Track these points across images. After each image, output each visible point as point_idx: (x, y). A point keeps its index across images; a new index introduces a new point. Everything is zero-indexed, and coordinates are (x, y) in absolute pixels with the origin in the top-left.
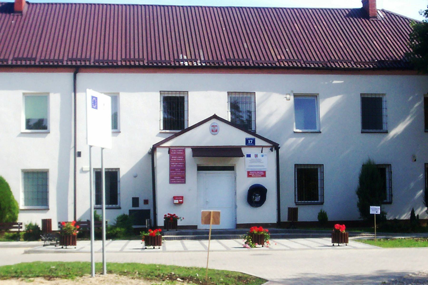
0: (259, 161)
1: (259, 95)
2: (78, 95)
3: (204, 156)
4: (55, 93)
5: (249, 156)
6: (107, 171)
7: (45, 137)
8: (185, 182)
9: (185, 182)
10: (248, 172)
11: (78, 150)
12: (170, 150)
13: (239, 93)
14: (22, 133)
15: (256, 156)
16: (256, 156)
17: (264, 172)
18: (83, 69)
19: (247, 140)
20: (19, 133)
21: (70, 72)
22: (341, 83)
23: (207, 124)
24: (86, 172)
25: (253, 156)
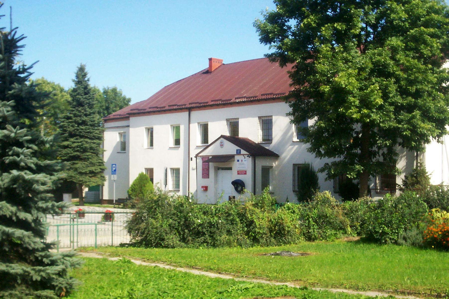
0: (243, 164)
1: (274, 118)
2: (191, 125)
3: (217, 162)
4: (182, 125)
5: (238, 161)
6: (263, 167)
7: (178, 150)
8: (209, 178)
9: (209, 178)
10: (238, 171)
11: (190, 157)
12: (203, 157)
13: (264, 116)
14: (170, 148)
15: (242, 161)
16: (242, 161)
17: (246, 171)
18: (193, 109)
19: (237, 150)
20: (168, 148)
21: (186, 111)
22: (176, 130)
23: (219, 142)
24: (195, 169)
25: (240, 161)
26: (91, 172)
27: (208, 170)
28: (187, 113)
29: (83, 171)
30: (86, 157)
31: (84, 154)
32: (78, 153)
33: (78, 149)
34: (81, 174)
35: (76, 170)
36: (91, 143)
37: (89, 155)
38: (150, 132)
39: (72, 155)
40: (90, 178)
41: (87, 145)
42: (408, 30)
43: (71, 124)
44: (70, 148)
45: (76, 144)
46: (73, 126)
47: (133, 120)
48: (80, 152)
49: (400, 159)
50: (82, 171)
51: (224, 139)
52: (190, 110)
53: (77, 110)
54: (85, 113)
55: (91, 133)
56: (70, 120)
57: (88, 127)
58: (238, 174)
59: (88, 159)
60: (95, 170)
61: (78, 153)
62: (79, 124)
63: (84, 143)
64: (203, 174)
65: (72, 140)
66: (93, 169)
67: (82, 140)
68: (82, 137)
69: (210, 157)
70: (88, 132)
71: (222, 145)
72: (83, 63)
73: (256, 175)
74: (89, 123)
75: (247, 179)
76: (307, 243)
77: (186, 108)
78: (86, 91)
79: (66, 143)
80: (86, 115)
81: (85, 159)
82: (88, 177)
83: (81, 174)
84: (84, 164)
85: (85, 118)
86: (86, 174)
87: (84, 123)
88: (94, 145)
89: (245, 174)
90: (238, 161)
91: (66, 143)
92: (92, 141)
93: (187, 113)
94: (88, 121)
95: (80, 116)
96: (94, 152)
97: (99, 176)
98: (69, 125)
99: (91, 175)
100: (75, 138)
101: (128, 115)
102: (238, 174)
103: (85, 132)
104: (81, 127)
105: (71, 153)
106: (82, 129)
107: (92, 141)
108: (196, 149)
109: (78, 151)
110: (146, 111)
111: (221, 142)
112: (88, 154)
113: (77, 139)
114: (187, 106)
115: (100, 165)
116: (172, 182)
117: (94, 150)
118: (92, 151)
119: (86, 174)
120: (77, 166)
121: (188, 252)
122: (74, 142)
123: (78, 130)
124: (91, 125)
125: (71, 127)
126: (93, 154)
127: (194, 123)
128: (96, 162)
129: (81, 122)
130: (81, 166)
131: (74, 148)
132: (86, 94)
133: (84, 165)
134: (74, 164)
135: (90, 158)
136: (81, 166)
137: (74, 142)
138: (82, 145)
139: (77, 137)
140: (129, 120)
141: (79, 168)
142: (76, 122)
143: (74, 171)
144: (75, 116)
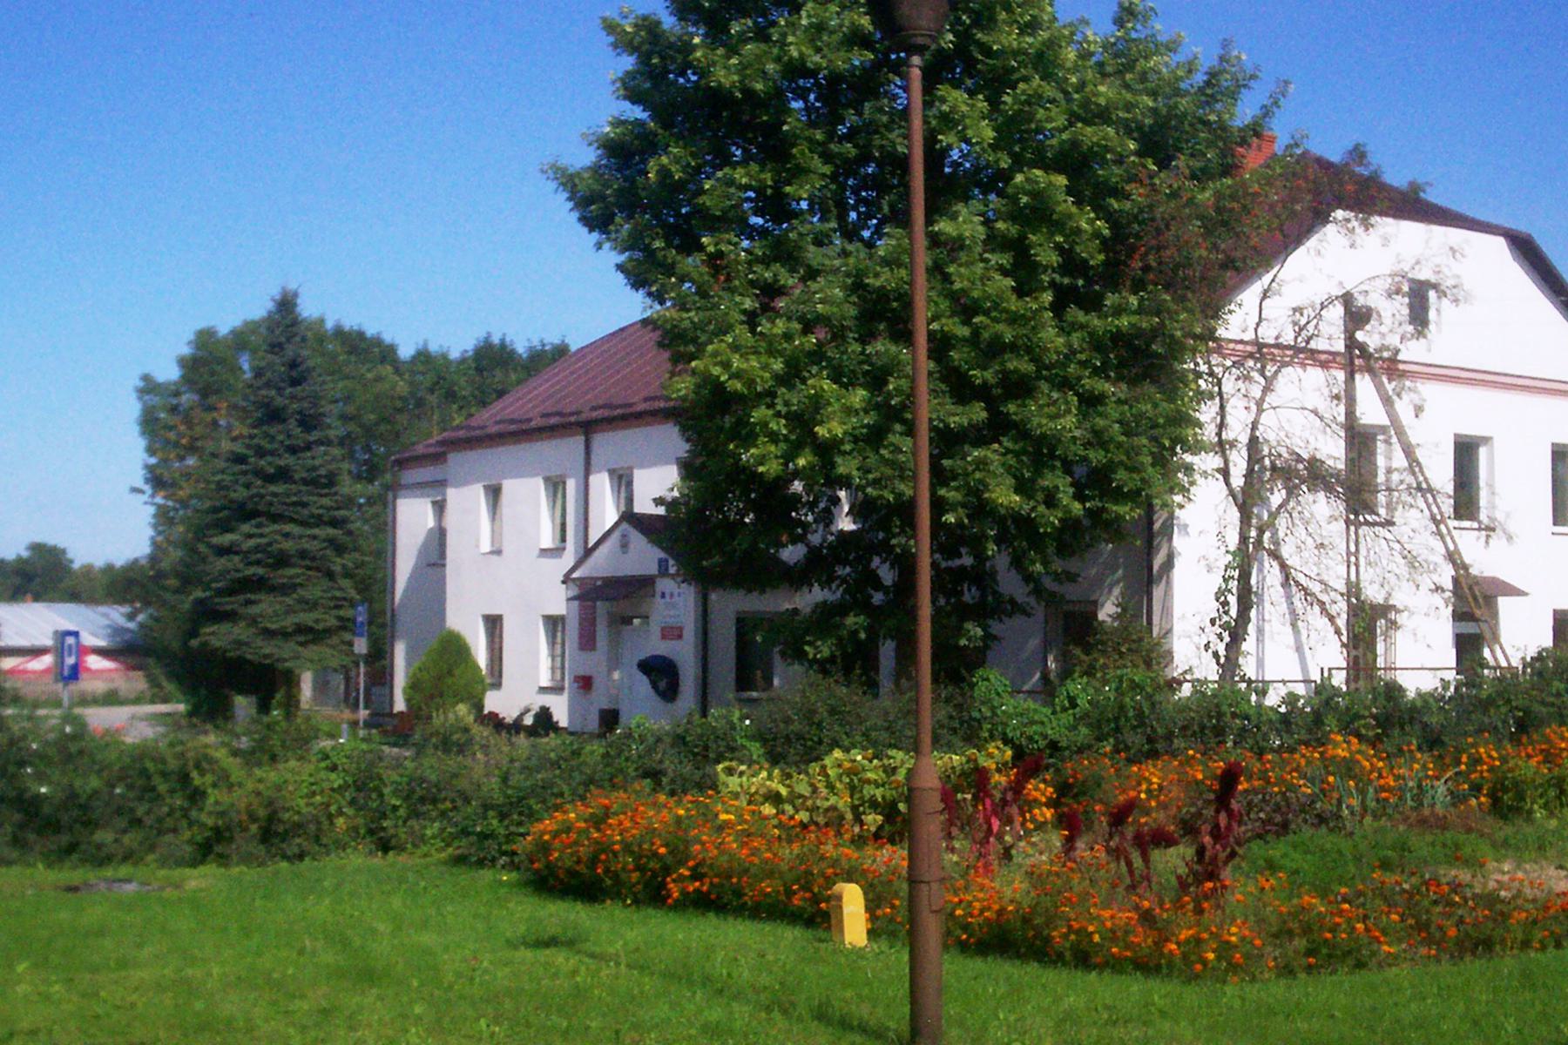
20: (537, 552)
25: (667, 596)
26: (301, 629)
27: (593, 623)
28: (581, 439)
29: (274, 627)
30: (285, 581)
31: (280, 572)
32: (260, 571)
33: (259, 556)
34: (269, 634)
35: (253, 621)
36: (301, 537)
37: (298, 576)
38: (623, 495)
39: (241, 575)
40: (300, 649)
41: (288, 545)
42: (1006, 176)
43: (242, 479)
44: (236, 553)
45: (252, 543)
46: (248, 486)
47: (454, 458)
48: (267, 566)
49: (1106, 590)
50: (269, 625)
51: (635, 527)
52: (588, 428)
53: (266, 435)
54: (287, 443)
55: (304, 505)
56: (244, 467)
57: (293, 486)
58: (664, 637)
59: (294, 587)
60: (317, 621)
61: (260, 571)
62: (269, 479)
63: (278, 537)
64: (580, 644)
65: (246, 528)
66: (307, 618)
67: (276, 527)
68: (276, 518)
69: (599, 583)
70: (295, 504)
71: (624, 546)
72: (292, 286)
73: (710, 646)
74: (297, 477)
75: (684, 653)
76: (377, 861)
77: (579, 424)
78: (294, 374)
79: (227, 539)
80: (293, 450)
81: (286, 589)
82: (292, 645)
83: (269, 634)
84: (280, 603)
85: (288, 460)
86: (284, 634)
87: (283, 475)
88: (315, 542)
89: (680, 637)
90: (663, 596)
91: (227, 539)
92: (309, 532)
93: (578, 441)
94: (297, 467)
95: (273, 453)
96: (314, 564)
97: (335, 640)
98: (237, 482)
99: (302, 639)
100: (253, 522)
101: (439, 449)
102: (664, 637)
103: (285, 504)
104: (273, 488)
105: (237, 571)
106: (275, 495)
107: (309, 532)
108: (539, 556)
109: (258, 563)
110: (533, 424)
111: (624, 536)
112: (292, 571)
113: (259, 526)
114: (583, 417)
115: (337, 607)
116: (550, 660)
117: (313, 559)
118: (308, 562)
119: (284, 634)
120: (254, 610)
121: (1480, 915)
122: (250, 536)
123: (262, 496)
124: (305, 482)
125: (241, 489)
126: (310, 573)
127: (599, 472)
128: (322, 598)
129: (272, 471)
130: (270, 611)
131: (248, 552)
132: (295, 382)
133: (278, 607)
134: (249, 602)
135: (301, 585)
136: (270, 611)
137: (250, 536)
138: (270, 544)
139: (258, 520)
140: (445, 461)
141: (261, 616)
142: (259, 473)
143: (249, 625)
144: (261, 453)
